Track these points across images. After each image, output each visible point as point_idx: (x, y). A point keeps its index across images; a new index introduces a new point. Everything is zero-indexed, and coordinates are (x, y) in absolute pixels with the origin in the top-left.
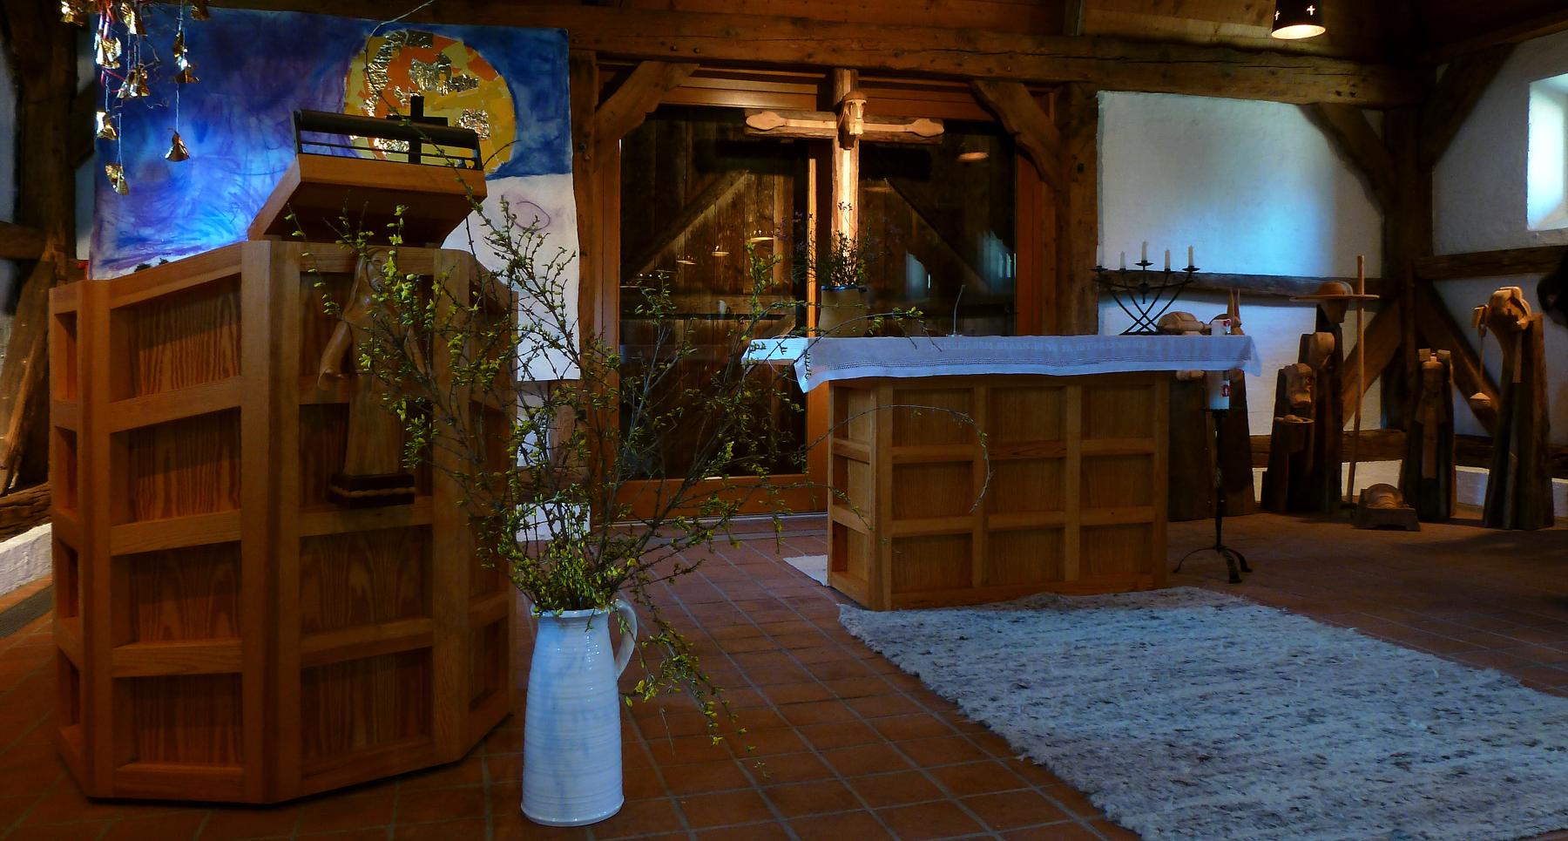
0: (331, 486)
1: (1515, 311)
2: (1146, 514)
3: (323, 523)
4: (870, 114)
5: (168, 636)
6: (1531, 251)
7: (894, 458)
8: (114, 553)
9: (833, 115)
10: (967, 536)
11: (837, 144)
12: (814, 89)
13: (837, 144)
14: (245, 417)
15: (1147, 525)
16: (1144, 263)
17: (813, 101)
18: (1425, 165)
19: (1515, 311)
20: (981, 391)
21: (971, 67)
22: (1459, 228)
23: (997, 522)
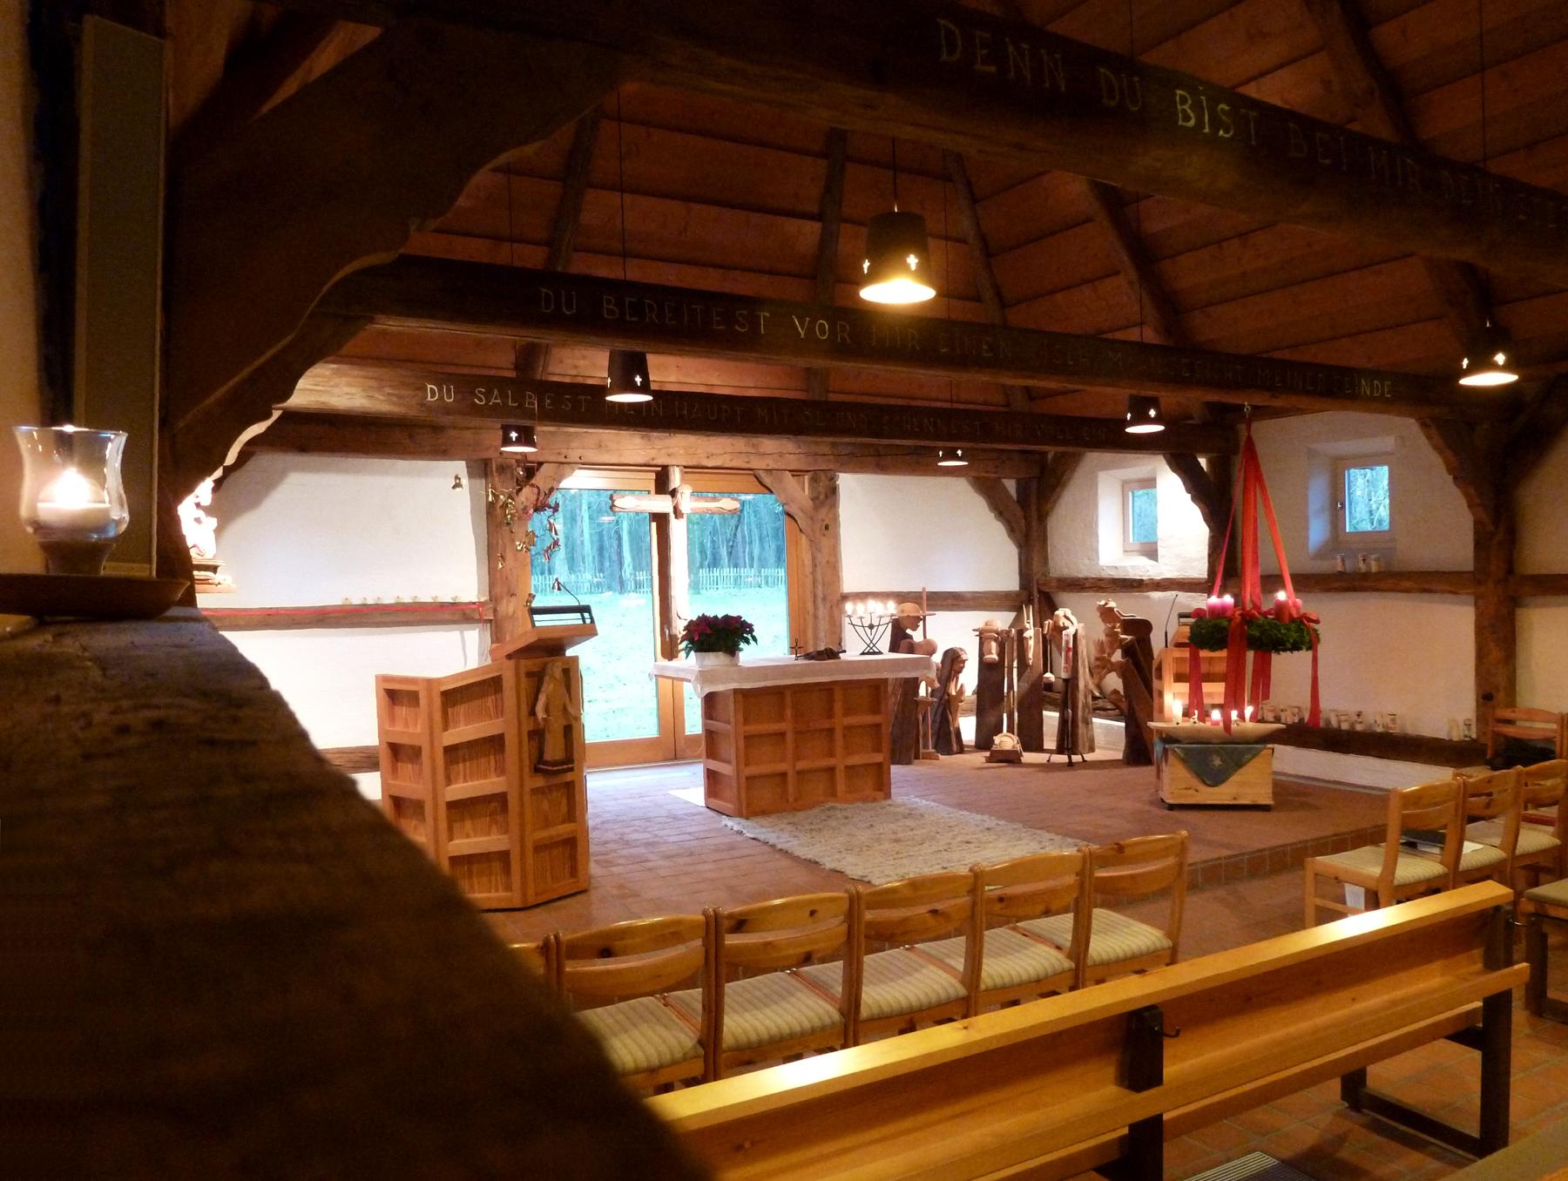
0: (539, 766)
1: (1067, 623)
2: (878, 758)
3: (540, 782)
4: (697, 493)
5: (468, 836)
6: (1101, 580)
7: (1404, 817)
8: (449, 799)
9: (669, 497)
10: (784, 775)
11: (672, 516)
12: (653, 476)
13: (672, 516)
14: (507, 737)
15: (879, 765)
16: (1008, 405)
17: (652, 487)
18: (1043, 517)
19: (1067, 623)
20: (788, 694)
21: (757, 463)
22: (1064, 560)
23: (801, 765)
